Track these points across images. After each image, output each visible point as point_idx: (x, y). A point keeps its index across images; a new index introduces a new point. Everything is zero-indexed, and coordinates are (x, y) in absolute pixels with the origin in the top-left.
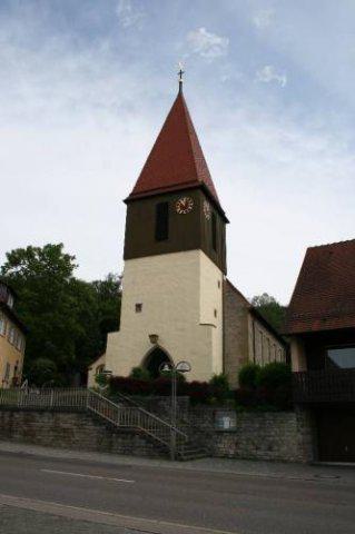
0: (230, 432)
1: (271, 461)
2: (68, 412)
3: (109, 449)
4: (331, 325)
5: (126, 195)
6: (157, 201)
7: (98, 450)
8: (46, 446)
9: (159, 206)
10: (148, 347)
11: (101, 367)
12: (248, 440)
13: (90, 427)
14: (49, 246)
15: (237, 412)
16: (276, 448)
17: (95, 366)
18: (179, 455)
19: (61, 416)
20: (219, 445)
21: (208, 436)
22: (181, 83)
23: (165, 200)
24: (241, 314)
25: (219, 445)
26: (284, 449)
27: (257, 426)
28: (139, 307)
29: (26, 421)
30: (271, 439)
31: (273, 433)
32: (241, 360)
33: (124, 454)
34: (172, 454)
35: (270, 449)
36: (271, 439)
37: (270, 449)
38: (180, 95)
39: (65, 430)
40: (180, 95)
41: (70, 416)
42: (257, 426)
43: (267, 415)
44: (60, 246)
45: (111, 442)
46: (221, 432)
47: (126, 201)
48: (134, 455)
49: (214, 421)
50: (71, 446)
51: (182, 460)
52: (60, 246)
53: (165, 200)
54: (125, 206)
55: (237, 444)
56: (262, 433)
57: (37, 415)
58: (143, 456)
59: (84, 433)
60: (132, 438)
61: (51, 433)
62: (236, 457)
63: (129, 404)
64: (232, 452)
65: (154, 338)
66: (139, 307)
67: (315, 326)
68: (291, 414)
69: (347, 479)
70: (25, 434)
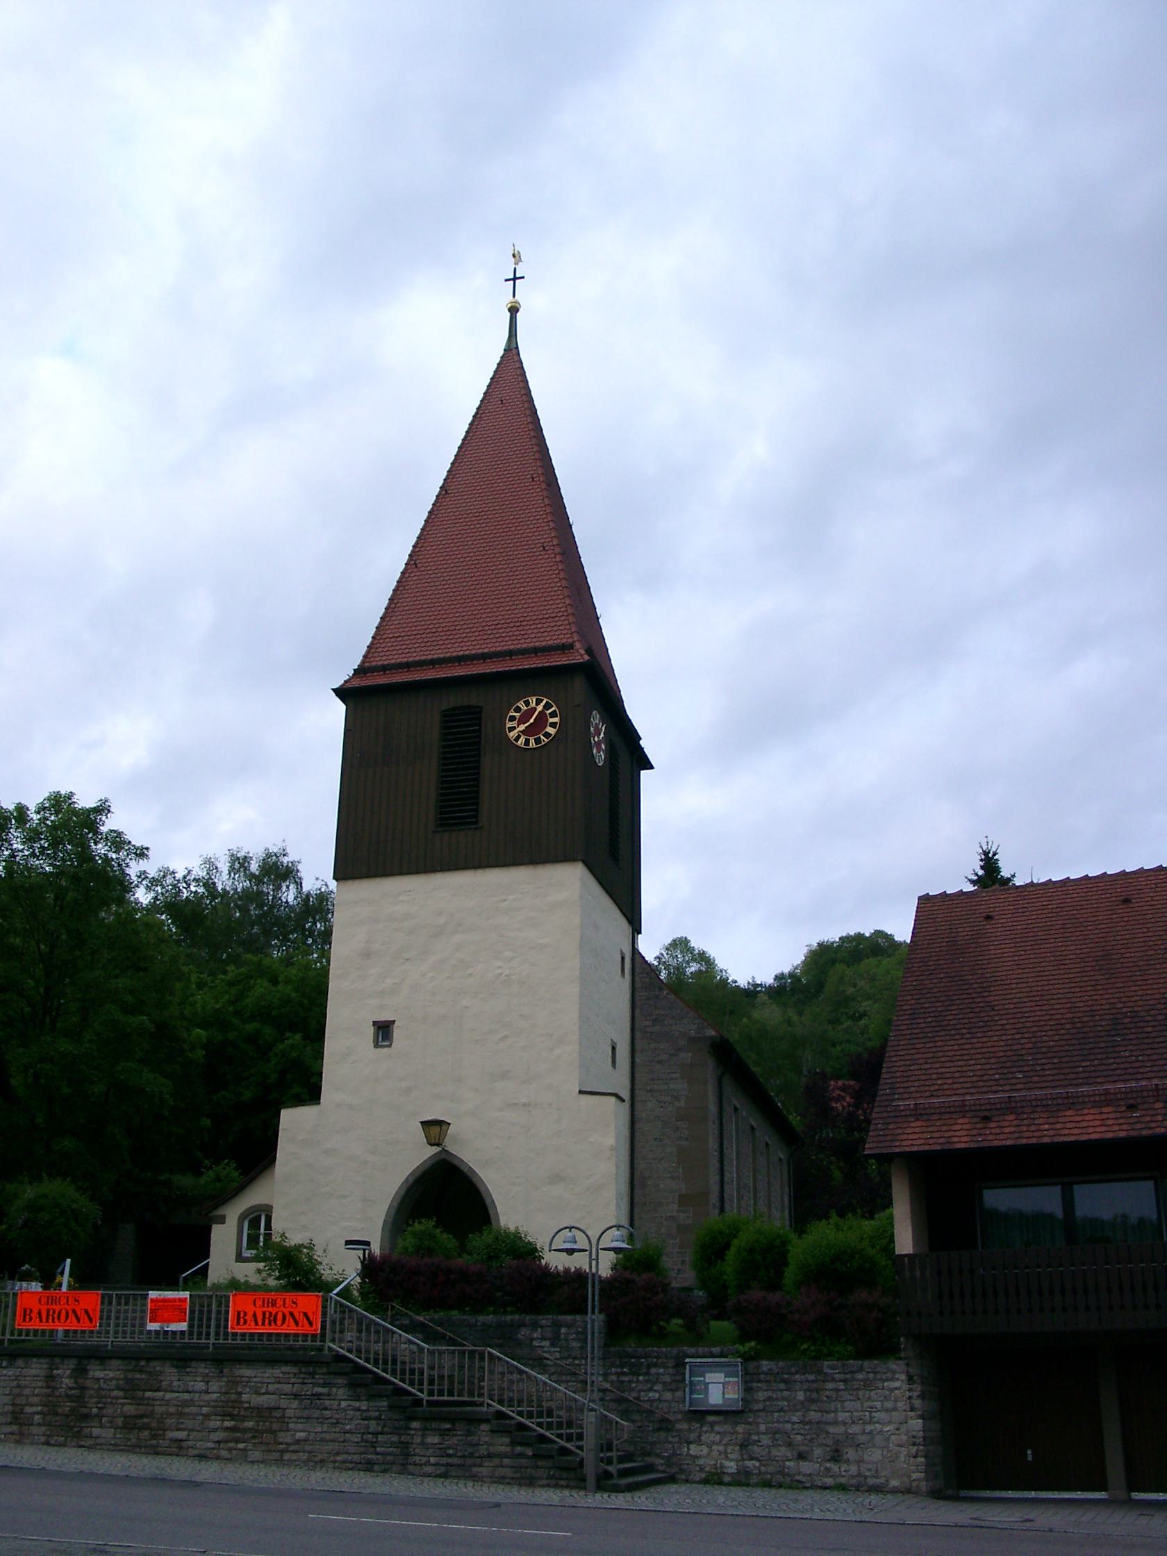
0: (725, 1413)
1: (843, 1488)
2: (271, 1362)
3: (402, 1463)
4: (1004, 1134)
5: (342, 673)
6: (453, 700)
7: (368, 1467)
8: (202, 1457)
9: (449, 717)
10: (419, 1154)
11: (258, 1219)
12: (774, 1433)
13: (341, 1399)
14: (59, 802)
15: (747, 1358)
16: (851, 1454)
17: (233, 1212)
18: (608, 1475)
19: (246, 1372)
20: (694, 1450)
21: (665, 1425)
22: (514, 310)
23: (472, 698)
24: (686, 1057)
25: (694, 1450)
26: (875, 1455)
27: (800, 1396)
28: (384, 1031)
29: (131, 1389)
30: (840, 1429)
31: (842, 1416)
32: (684, 1200)
33: (445, 1476)
34: (590, 1470)
35: (836, 1456)
36: (840, 1429)
37: (836, 1456)
38: (511, 355)
39: (261, 1413)
40: (511, 355)
41: (277, 1372)
42: (800, 1396)
43: (826, 1365)
44: (103, 809)
45: (552, 1457)
46: (700, 1415)
47: (341, 693)
48: (475, 1478)
49: (678, 1383)
50: (279, 1455)
51: (617, 1489)
52: (103, 809)
53: (472, 698)
54: (339, 709)
55: (744, 1445)
56: (814, 1415)
57: (170, 1374)
58: (501, 1480)
59: (789, 1437)
60: (469, 1433)
61: (215, 1423)
62: (742, 1480)
63: (431, 1336)
64: (731, 1467)
65: (435, 1128)
66: (384, 1031)
67: (962, 1136)
68: (893, 1365)
69: (1157, 1524)
70: (130, 1424)
